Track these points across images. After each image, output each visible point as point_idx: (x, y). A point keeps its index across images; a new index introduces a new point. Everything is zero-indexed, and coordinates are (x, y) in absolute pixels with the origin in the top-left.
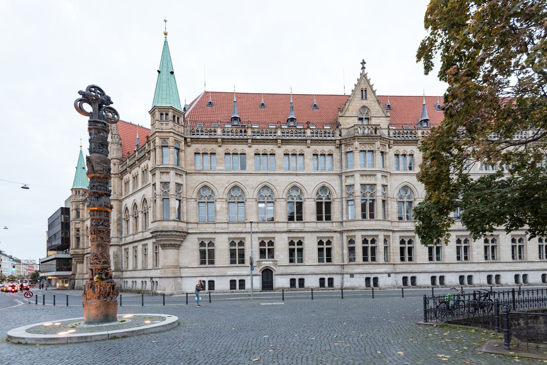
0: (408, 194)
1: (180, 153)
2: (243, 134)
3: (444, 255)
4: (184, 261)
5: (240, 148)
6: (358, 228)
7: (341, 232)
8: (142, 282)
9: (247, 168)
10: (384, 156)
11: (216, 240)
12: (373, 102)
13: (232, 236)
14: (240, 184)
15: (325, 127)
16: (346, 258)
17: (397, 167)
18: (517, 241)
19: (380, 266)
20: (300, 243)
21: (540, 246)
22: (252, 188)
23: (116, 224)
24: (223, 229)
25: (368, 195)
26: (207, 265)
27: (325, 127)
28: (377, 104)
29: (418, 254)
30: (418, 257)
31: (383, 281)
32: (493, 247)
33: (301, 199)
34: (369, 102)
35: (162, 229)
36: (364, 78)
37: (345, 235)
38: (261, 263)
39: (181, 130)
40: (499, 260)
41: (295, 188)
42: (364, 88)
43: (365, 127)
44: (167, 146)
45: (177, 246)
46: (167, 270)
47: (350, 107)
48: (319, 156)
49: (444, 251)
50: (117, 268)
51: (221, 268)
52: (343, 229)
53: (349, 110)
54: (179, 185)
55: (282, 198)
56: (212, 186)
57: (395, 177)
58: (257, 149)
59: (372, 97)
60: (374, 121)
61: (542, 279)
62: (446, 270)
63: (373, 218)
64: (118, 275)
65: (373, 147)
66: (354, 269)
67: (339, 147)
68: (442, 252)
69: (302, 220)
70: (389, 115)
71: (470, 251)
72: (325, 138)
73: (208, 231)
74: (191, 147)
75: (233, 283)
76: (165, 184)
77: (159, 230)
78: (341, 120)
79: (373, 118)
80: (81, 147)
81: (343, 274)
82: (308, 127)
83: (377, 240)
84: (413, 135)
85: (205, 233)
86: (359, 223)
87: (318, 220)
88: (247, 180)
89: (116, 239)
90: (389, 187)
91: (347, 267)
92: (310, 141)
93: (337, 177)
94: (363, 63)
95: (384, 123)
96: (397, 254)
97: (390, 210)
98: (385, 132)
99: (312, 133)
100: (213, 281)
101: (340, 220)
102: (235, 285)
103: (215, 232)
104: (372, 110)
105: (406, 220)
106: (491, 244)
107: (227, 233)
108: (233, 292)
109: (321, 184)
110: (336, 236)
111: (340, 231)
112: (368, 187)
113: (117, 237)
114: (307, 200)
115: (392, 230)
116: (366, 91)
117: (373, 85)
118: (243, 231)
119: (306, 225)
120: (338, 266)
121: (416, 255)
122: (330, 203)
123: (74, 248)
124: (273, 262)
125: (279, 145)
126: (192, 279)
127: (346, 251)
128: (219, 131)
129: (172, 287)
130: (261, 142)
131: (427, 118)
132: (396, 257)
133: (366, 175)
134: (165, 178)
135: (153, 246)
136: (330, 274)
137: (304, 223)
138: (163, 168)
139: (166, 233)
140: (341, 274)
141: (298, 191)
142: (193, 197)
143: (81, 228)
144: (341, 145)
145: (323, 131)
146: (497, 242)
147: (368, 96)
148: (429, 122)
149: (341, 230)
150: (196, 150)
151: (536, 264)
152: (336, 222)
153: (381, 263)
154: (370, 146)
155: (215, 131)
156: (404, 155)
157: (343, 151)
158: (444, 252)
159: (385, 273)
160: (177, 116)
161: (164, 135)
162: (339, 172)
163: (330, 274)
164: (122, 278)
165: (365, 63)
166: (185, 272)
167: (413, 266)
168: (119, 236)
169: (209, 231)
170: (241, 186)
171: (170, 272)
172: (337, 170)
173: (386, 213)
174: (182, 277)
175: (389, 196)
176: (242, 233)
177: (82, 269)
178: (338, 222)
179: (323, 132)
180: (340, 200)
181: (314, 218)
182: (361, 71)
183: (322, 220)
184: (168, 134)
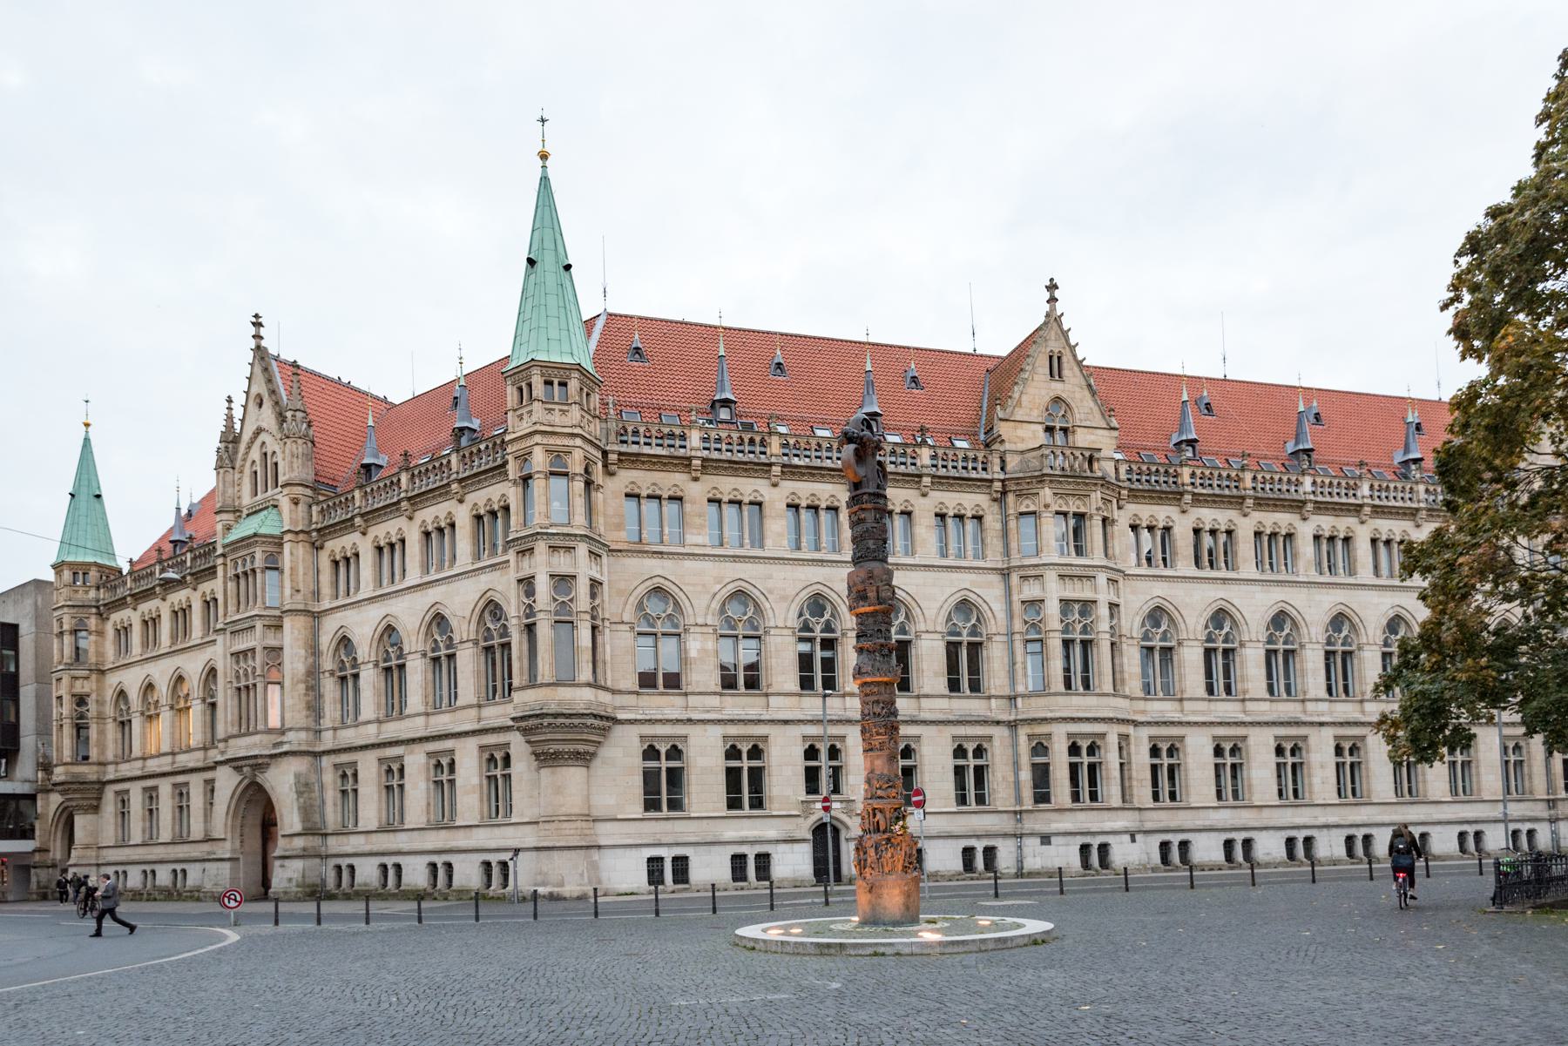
0: (1164, 628)
1: (593, 494)
2: (758, 449)
3: (1250, 786)
4: (605, 801)
5: (749, 487)
6: (1058, 715)
7: (1013, 725)
8: (175, 871)
9: (769, 542)
10: (1109, 529)
11: (691, 741)
12: (1077, 389)
13: (733, 730)
14: (751, 588)
15: (819, 433)
16: (1028, 793)
17: (941, 547)
18: (1288, 753)
19: (1114, 813)
20: (675, 753)
21: (1278, 765)
22: (783, 598)
23: (302, 687)
24: (708, 711)
25: (1079, 627)
26: (665, 812)
27: (819, 433)
28: (1087, 393)
29: (1191, 782)
30: (1192, 791)
31: (1124, 853)
32: (1171, 769)
33: (756, 629)
34: (1068, 387)
35: (560, 710)
36: (1055, 324)
37: (1023, 732)
38: (812, 806)
39: (596, 428)
40: (1369, 797)
41: (740, 595)
42: (1056, 351)
43: (1058, 452)
44: (566, 474)
45: (584, 758)
46: (565, 825)
47: (1024, 398)
48: (724, 507)
49: (1249, 774)
50: (309, 825)
51: (705, 821)
52: (1019, 717)
53: (1024, 404)
54: (595, 584)
55: (936, 632)
56: (677, 590)
57: (1134, 583)
58: (793, 493)
59: (1075, 376)
60: (1082, 439)
61: (1161, 853)
62: (1256, 824)
63: (959, 691)
64: (314, 848)
65: (1085, 505)
66: (1051, 821)
67: (1000, 499)
68: (1245, 776)
69: (678, 687)
70: (1117, 426)
71: (1245, 773)
72: (964, 474)
73: (671, 717)
74: (615, 479)
75: (738, 861)
76: (563, 581)
77: (550, 712)
78: (1003, 429)
79: (1078, 429)
80: (87, 425)
81: (1021, 836)
82: (924, 442)
83: (843, 748)
84: (1171, 480)
85: (661, 720)
86: (1060, 699)
87: (803, 687)
88: (770, 577)
89: (303, 735)
90: (1122, 608)
91: (1032, 816)
92: (929, 479)
93: (995, 579)
94: (1052, 287)
95: (1105, 442)
96: (1144, 783)
97: (1126, 668)
98: (1109, 467)
99: (786, 445)
100: (686, 858)
101: (1007, 692)
102: (662, 872)
103: (690, 721)
104: (1076, 410)
105: (1284, 696)
106: (1166, 761)
107: (719, 722)
108: (742, 889)
109: (959, 595)
110: (1000, 733)
111: (1010, 722)
112: (1077, 606)
113: (307, 729)
114: (924, 636)
115: (1133, 721)
116: (1059, 358)
117: (1077, 344)
118: (763, 718)
119: (925, 702)
120: (1005, 816)
121: (1187, 786)
122: (909, 642)
123: (69, 760)
124: (844, 805)
125: (774, 480)
126: (628, 852)
127: (1026, 776)
128: (695, 438)
129: (582, 875)
130: (803, 475)
131: (1193, 436)
132: (1142, 793)
133: (1071, 577)
134: (563, 564)
135: (481, 757)
136: (1476, 822)
137: (918, 697)
138: (558, 534)
139: (568, 721)
140: (1015, 836)
141: (746, 606)
142: (626, 618)
143: (94, 696)
144: (1004, 493)
145: (813, 442)
146: (1362, 753)
147: (1066, 372)
148: (1314, 456)
149: (1012, 718)
150: (630, 486)
151: (1445, 807)
152: (996, 697)
153: (1115, 805)
154: (1078, 502)
155: (683, 437)
156: (814, 508)
157: (1011, 511)
158: (1249, 779)
159: (1126, 832)
160: (585, 390)
161: (559, 442)
162: (1000, 566)
163: (1476, 822)
164: (327, 856)
165: (1056, 287)
166: (607, 833)
167: (1182, 813)
168: (312, 725)
169: (673, 717)
170: (755, 591)
171: (572, 832)
172: (994, 558)
173: (1118, 676)
174: (599, 847)
175: (1124, 632)
176: (760, 721)
177: (95, 833)
178: (1002, 697)
179: (814, 446)
180: (1004, 638)
181: (941, 684)
182: (1047, 307)
183: (655, 686)
184: (567, 441)
